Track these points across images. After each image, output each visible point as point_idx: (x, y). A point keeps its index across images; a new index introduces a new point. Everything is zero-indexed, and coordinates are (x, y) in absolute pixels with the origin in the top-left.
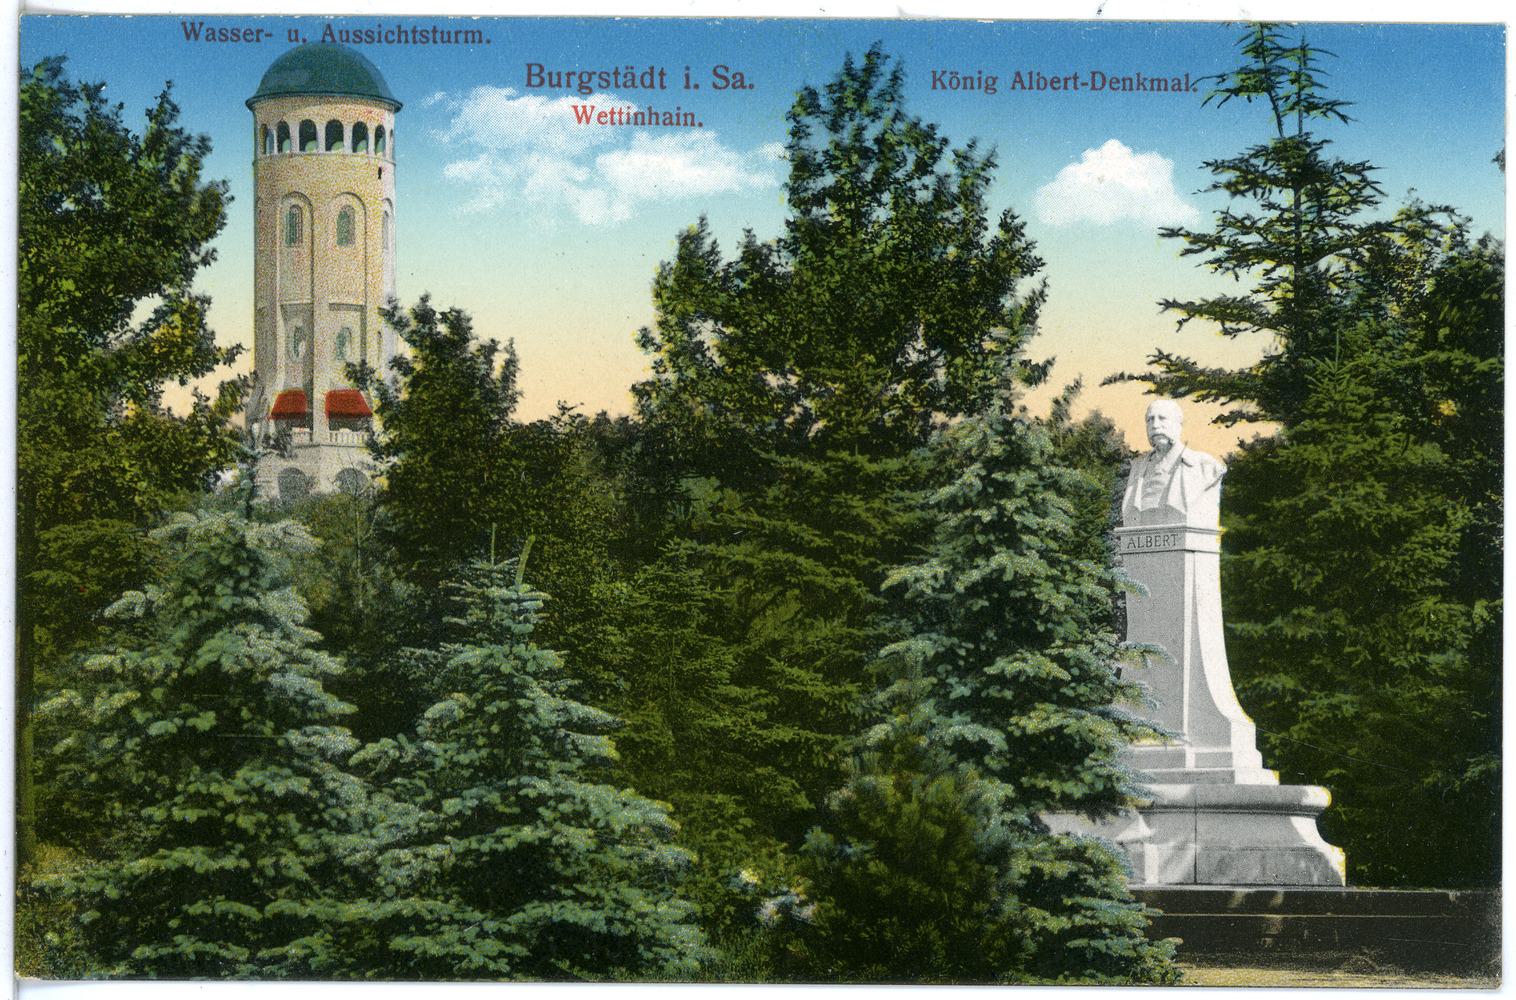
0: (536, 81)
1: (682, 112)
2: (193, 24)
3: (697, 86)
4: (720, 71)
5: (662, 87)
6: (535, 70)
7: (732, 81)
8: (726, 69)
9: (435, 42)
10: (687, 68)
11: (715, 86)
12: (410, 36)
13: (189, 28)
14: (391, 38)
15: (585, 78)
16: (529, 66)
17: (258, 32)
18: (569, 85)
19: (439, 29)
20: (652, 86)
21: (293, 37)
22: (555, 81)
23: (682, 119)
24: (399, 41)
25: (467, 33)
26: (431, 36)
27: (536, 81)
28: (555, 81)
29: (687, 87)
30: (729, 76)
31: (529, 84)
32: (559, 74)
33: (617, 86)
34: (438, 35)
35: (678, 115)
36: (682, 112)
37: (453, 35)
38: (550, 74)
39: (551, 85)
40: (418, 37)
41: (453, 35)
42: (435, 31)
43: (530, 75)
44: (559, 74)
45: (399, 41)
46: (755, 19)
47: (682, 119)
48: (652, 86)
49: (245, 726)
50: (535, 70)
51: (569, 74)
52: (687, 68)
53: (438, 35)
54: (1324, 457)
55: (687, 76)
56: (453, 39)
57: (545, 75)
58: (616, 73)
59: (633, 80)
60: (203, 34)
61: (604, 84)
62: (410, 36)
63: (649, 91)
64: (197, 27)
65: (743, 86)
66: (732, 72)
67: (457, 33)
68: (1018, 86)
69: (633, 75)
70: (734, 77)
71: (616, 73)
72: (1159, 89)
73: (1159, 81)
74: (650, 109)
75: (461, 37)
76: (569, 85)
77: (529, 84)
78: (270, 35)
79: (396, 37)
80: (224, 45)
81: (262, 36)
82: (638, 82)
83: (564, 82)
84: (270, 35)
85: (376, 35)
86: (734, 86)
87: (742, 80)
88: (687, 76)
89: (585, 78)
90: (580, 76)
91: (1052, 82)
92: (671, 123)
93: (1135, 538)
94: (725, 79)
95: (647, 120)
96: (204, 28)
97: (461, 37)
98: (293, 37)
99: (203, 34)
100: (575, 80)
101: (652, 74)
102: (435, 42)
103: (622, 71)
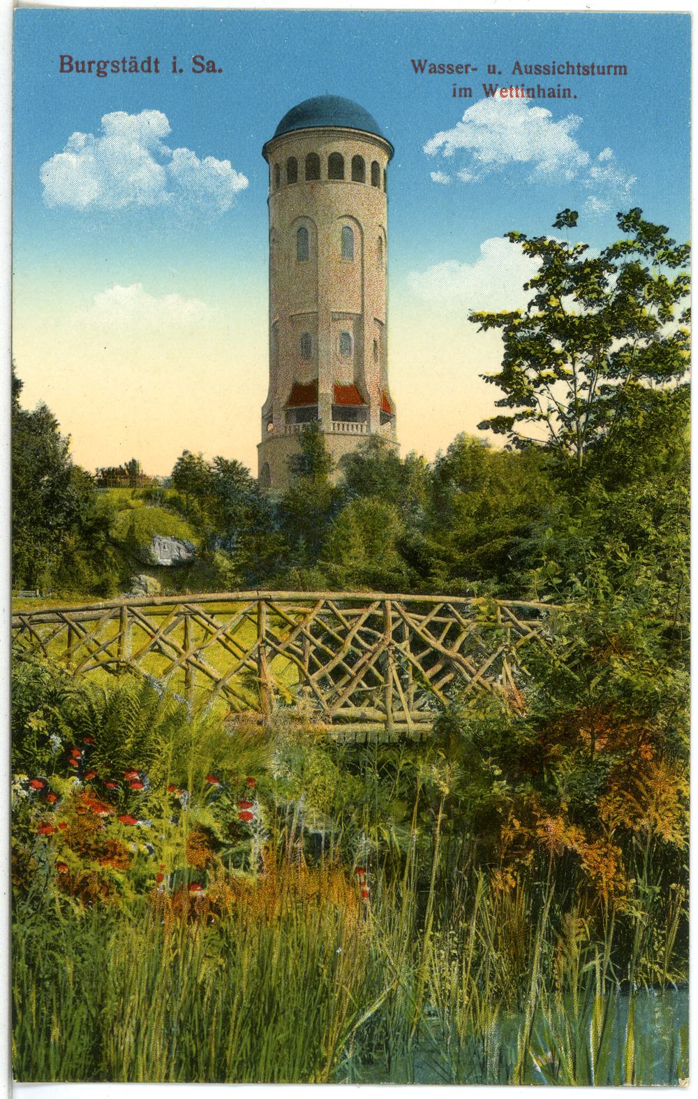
0: (67, 67)
1: (561, 88)
3: (500, 73)
4: (198, 60)
5: (157, 71)
6: (66, 60)
8: (202, 58)
10: (175, 58)
12: (576, 69)
13: (417, 63)
15: (102, 65)
16: (62, 57)
17: (467, 66)
20: (149, 71)
23: (562, 93)
24: (568, 73)
25: (615, 67)
26: (590, 70)
27: (67, 67)
29: (174, 71)
30: (205, 64)
31: (62, 71)
32: (83, 63)
34: (595, 69)
36: (561, 88)
37: (606, 69)
38: (77, 63)
39: (78, 71)
40: (581, 70)
41: (606, 69)
43: (62, 64)
45: (568, 73)
47: (562, 93)
48: (149, 71)
49: (481, 876)
50: (66, 60)
51: (90, 63)
52: (175, 58)
53: (595, 69)
55: (174, 64)
57: (73, 63)
58: (124, 61)
60: (427, 68)
62: (576, 69)
64: (423, 63)
65: (214, 70)
66: (207, 60)
68: (517, 71)
70: (208, 63)
71: (124, 61)
73: (620, 67)
74: (539, 86)
75: (612, 70)
77: (62, 71)
78: (475, 69)
79: (566, 69)
80: (538, 76)
81: (469, 70)
84: (475, 69)
85: (551, 69)
86: (208, 71)
87: (213, 66)
88: (174, 64)
89: (102, 65)
90: (98, 65)
91: (457, 68)
92: (554, 96)
93: (359, 432)
94: (202, 65)
95: (536, 94)
96: (428, 64)
97: (612, 70)
99: (427, 68)
100: (94, 67)
101: (149, 64)
102: (593, 74)
103: (128, 60)
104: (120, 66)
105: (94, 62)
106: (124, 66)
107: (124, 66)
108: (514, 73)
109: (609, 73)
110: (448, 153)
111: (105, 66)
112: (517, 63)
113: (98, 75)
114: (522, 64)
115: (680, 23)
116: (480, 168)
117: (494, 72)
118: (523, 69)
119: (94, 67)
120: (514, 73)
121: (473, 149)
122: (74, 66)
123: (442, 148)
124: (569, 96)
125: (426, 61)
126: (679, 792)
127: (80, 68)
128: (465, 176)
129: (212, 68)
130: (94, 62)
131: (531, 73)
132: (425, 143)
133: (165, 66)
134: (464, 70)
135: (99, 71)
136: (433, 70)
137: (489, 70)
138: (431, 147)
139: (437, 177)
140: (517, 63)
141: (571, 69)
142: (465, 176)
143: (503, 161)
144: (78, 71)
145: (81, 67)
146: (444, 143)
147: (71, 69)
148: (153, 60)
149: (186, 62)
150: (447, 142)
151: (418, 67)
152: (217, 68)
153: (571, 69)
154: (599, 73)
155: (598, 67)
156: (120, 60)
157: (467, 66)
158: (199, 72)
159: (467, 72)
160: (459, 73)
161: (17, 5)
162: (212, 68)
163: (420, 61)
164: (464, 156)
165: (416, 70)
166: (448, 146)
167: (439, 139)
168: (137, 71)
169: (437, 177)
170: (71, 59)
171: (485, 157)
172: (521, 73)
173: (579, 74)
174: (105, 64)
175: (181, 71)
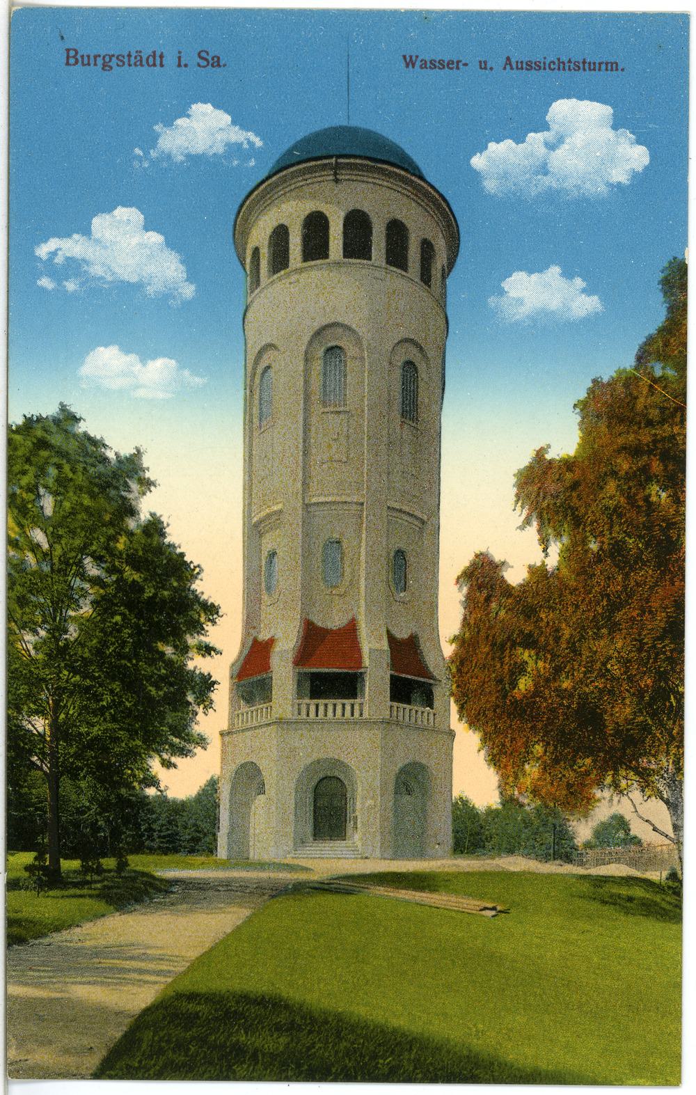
0: (72, 61)
2: (411, 57)
4: (203, 55)
5: (162, 65)
6: (72, 53)
7: (211, 62)
9: (584, 70)
11: (199, 65)
13: (408, 60)
14: (552, 66)
15: (107, 59)
16: (68, 50)
17: (458, 62)
18: (95, 64)
19: (588, 60)
20: (154, 65)
21: (483, 66)
22: (86, 62)
25: (607, 64)
26: (581, 66)
27: (72, 61)
28: (86, 62)
29: (179, 65)
30: (210, 59)
31: (68, 64)
32: (88, 56)
33: (130, 65)
34: (587, 65)
35: (544, 63)
37: (597, 65)
38: (82, 57)
41: (597, 65)
42: (584, 62)
43: (68, 57)
44: (88, 56)
45: (559, 69)
46: (121, 7)
50: (72, 53)
51: (600, 64)
52: (180, 52)
53: (587, 65)
54: (170, 1055)
55: (179, 58)
56: (597, 68)
57: (78, 57)
58: (129, 56)
59: (141, 61)
61: (121, 64)
62: (567, 65)
63: (87, 67)
64: (414, 58)
65: (219, 65)
66: (212, 54)
67: (600, 64)
68: (508, 67)
69: (141, 58)
71: (129, 56)
72: (612, 70)
73: (612, 64)
75: (603, 67)
76: (95, 64)
78: (466, 65)
80: (442, 72)
81: (460, 64)
82: (144, 62)
83: (92, 61)
84: (466, 65)
85: (542, 65)
88: (179, 58)
89: (107, 59)
91: (448, 64)
97: (603, 67)
98: (483, 66)
99: (418, 64)
100: (100, 61)
102: (584, 70)
103: (134, 54)
104: (126, 60)
105: (99, 56)
106: (129, 61)
107: (129, 61)
108: (505, 68)
109: (600, 70)
110: (59, 260)
111: (110, 61)
112: (508, 59)
113: (103, 69)
114: (513, 61)
115: (682, 20)
116: (87, 280)
117: (485, 68)
118: (514, 66)
119: (100, 61)
120: (505, 68)
121: (84, 260)
122: (80, 59)
123: (54, 254)
124: (617, 70)
125: (417, 57)
126: (50, 1043)
127: (520, 66)
128: (71, 286)
129: (217, 62)
130: (99, 56)
131: (522, 68)
132: (38, 244)
133: (170, 60)
134: (455, 65)
135: (104, 65)
136: (424, 65)
137: (481, 66)
138: (43, 251)
139: (45, 282)
140: (508, 59)
141: (562, 65)
142: (71, 286)
143: (109, 278)
144: (83, 64)
145: (87, 61)
146: (57, 250)
147: (77, 62)
148: (158, 54)
149: (191, 58)
150: (60, 249)
151: (410, 62)
152: (222, 63)
153: (562, 65)
154: (590, 69)
155: (590, 63)
156: (126, 54)
157: (458, 62)
158: (204, 67)
159: (458, 68)
160: (452, 69)
161: (12, 4)
162: (217, 62)
163: (411, 57)
164: (74, 267)
165: (407, 66)
166: (60, 253)
167: (53, 244)
168: (142, 65)
169: (45, 282)
170: (77, 53)
171: (97, 270)
172: (512, 68)
173: (569, 69)
174: (111, 57)
175: (186, 66)
